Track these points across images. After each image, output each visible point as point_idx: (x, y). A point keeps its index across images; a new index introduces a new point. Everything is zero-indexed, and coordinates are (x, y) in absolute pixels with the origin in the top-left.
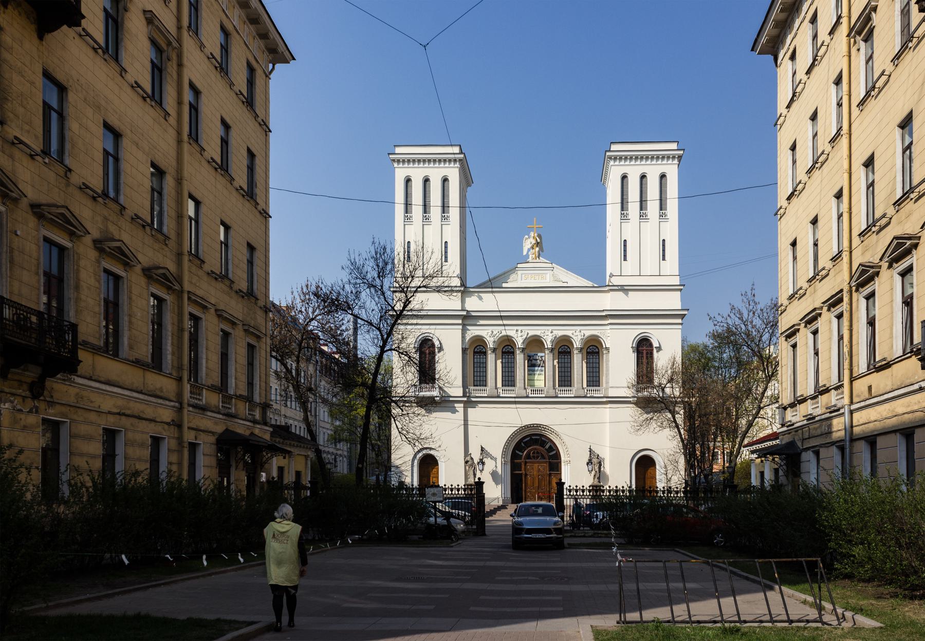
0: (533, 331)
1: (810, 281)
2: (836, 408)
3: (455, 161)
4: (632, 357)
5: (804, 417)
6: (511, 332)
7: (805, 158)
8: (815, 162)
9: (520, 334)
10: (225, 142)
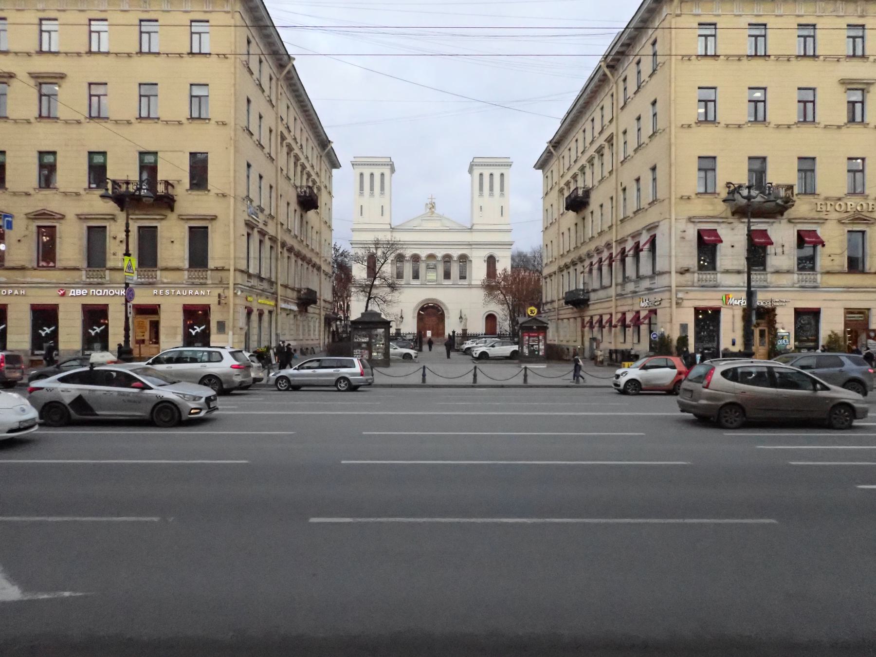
3: (388, 165)
7: (633, 144)
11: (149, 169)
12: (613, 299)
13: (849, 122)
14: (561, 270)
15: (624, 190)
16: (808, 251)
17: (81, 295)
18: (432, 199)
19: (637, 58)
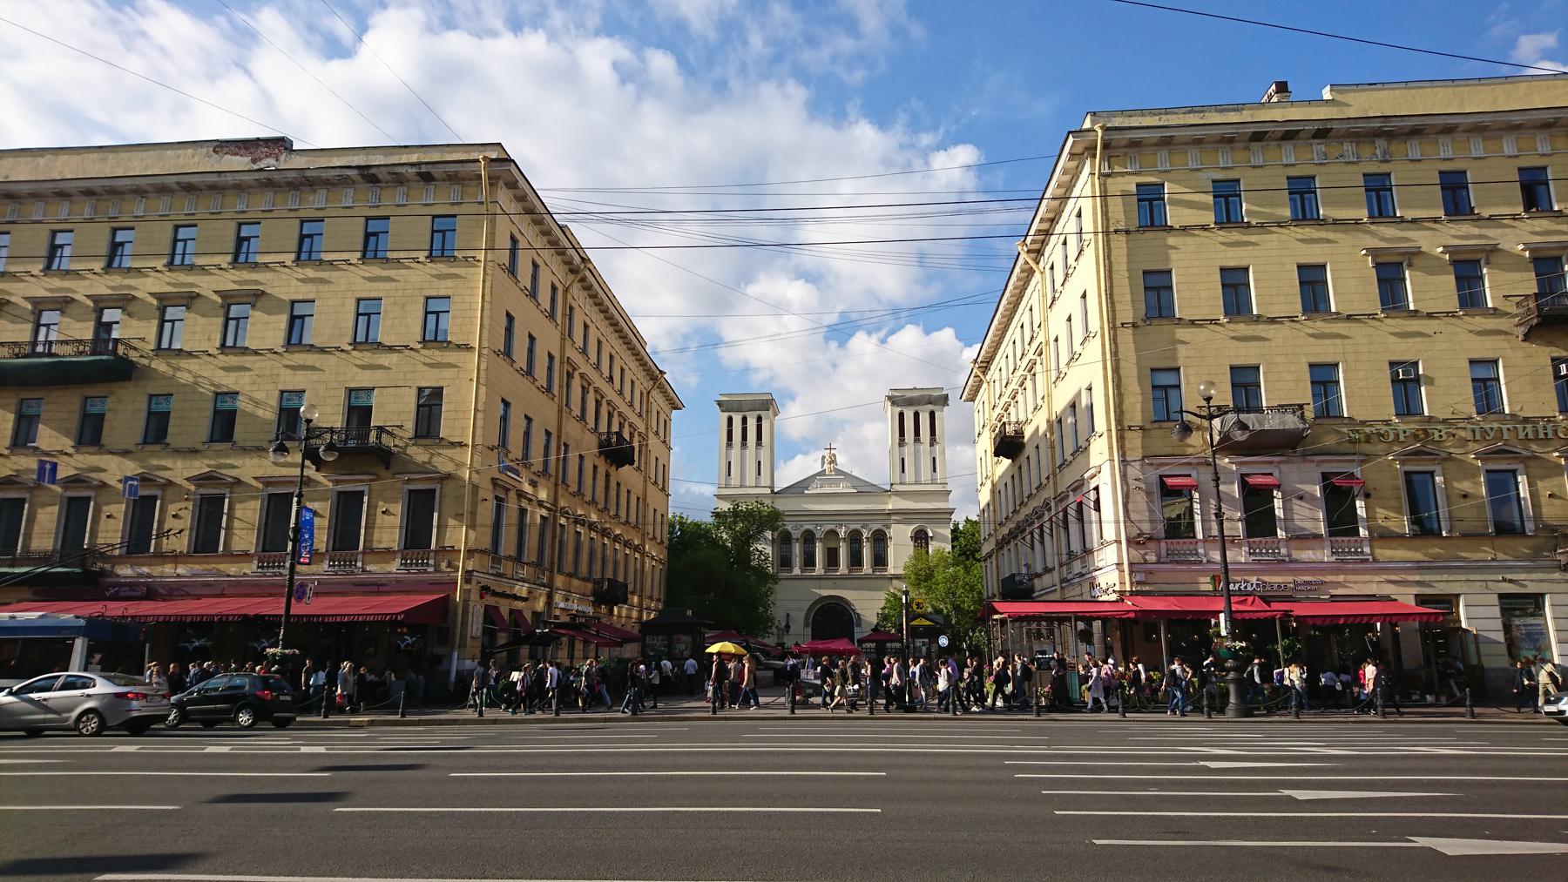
10: (531, 351)
11: (359, 414)
12: (1058, 587)
13: (1148, 318)
14: (1001, 544)
16: (1176, 509)
17: (1029, 622)
19: (1063, 237)
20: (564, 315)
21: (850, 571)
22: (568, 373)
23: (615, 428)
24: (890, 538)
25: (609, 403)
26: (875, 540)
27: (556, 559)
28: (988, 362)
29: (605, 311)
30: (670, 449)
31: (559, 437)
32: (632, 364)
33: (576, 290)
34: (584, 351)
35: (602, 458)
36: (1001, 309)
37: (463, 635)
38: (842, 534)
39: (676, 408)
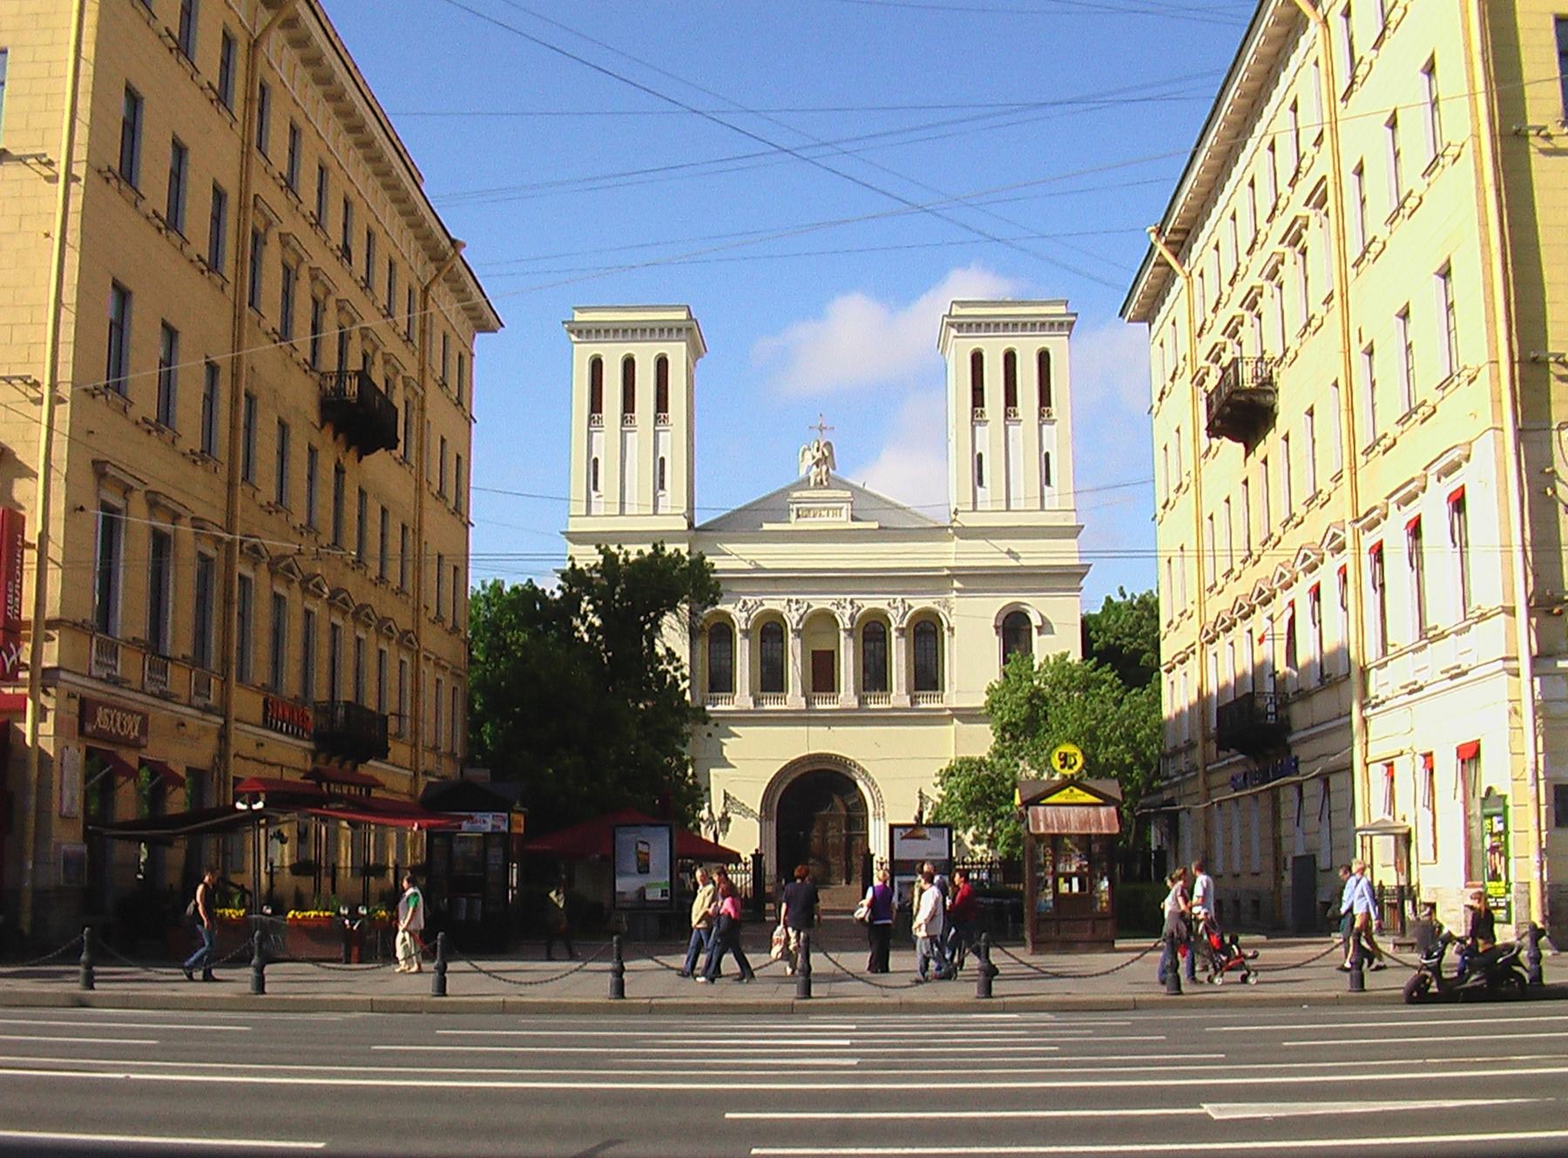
0: (821, 602)
1: (1442, 386)
2: (1459, 671)
4: (995, 643)
5: (1402, 688)
6: (775, 603)
7: (1381, 203)
8: (1366, 251)
9: (794, 606)
10: (177, 176)
15: (1370, 352)
18: (821, 429)
20: (248, 100)
21: (862, 701)
22: (255, 235)
23: (355, 363)
24: (951, 629)
25: (341, 306)
26: (916, 634)
27: (234, 654)
28: (1188, 232)
29: (335, 97)
30: (470, 419)
31: (235, 376)
32: (391, 222)
33: (277, 41)
34: (289, 184)
35: (328, 431)
36: (1225, 108)
37: (43, 811)
38: (844, 622)
39: (485, 328)
